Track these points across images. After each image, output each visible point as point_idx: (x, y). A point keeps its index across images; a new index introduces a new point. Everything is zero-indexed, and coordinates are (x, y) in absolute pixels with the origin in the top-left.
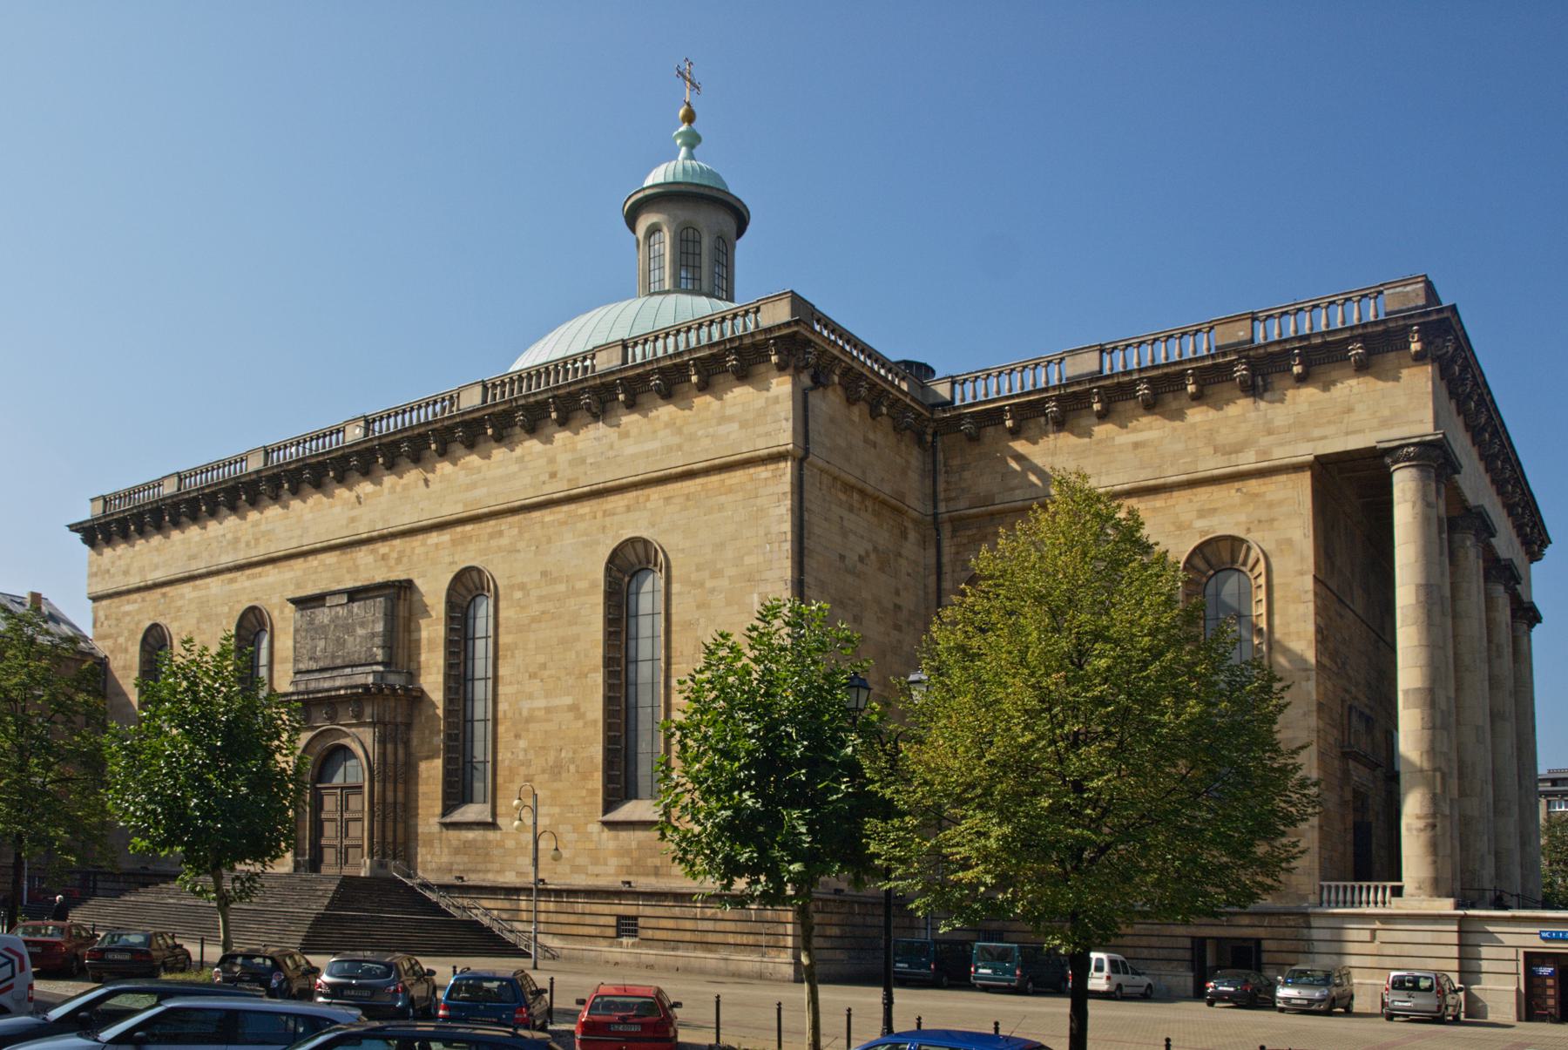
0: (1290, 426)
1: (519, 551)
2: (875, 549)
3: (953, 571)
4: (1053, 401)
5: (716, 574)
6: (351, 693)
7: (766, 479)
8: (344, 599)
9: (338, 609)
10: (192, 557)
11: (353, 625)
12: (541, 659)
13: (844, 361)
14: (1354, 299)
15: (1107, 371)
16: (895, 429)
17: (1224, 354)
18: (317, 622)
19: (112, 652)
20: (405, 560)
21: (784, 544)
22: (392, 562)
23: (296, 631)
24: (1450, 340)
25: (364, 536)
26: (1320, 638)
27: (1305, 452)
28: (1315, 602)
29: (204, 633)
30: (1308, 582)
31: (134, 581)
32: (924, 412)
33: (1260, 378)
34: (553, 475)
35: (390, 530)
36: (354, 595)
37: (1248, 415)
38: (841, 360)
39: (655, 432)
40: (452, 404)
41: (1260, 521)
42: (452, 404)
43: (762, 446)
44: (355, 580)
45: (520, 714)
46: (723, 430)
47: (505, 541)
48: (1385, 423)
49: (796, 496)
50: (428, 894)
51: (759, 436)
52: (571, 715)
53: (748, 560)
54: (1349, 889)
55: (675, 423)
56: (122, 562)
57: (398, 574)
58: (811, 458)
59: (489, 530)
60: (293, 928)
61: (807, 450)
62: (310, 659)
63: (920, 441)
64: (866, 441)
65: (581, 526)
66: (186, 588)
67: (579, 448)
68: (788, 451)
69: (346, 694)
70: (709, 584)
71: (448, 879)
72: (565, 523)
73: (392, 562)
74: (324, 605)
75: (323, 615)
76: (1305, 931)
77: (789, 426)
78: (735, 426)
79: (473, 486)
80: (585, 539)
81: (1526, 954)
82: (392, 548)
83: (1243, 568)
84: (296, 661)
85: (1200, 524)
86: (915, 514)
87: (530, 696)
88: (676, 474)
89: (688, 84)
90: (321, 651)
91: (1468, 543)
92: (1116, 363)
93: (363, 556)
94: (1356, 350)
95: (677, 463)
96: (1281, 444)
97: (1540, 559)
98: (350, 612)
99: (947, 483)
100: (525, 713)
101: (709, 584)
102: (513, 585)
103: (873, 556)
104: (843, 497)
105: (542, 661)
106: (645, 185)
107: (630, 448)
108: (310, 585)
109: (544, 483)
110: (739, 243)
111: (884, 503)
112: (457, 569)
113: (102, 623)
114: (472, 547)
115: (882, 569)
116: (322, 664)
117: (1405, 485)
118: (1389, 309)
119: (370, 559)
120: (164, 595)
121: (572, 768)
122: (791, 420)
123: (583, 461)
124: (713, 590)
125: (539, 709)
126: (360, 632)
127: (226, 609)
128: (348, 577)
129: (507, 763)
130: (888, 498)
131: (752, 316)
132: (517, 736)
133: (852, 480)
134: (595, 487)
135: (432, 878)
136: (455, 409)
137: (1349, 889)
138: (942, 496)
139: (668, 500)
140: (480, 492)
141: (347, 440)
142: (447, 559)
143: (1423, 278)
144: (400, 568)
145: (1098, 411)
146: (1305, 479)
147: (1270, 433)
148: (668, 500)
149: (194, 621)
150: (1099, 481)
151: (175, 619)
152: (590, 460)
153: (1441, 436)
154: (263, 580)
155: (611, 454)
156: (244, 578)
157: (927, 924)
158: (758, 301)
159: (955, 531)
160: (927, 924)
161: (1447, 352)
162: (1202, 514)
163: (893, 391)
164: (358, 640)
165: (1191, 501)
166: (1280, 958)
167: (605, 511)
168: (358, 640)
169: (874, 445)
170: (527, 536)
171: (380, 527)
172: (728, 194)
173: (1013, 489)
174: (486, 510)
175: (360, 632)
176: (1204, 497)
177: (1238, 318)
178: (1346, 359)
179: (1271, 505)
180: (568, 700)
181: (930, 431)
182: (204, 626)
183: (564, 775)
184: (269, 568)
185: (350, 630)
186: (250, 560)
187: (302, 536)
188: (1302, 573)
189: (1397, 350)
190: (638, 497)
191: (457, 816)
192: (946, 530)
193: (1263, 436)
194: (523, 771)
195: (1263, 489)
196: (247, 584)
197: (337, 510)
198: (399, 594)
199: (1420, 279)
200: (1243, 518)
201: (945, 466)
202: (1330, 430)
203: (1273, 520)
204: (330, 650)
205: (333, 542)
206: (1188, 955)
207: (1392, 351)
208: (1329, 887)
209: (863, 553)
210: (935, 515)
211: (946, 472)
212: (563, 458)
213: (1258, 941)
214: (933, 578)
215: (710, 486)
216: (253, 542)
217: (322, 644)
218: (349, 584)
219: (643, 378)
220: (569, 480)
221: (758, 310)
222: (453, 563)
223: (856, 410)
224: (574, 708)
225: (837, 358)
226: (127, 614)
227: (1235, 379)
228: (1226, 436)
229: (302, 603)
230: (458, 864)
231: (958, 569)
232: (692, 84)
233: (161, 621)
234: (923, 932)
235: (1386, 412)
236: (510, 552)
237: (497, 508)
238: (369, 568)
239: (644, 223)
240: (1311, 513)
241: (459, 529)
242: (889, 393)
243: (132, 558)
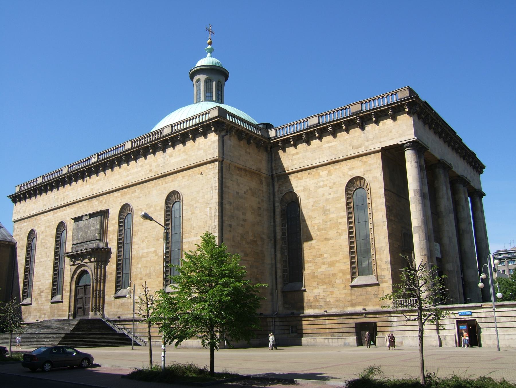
0: (374, 138)
1: (140, 197)
2: (250, 189)
3: (278, 194)
4: (330, 127)
5: (197, 202)
6: (88, 251)
7: (211, 168)
8: (88, 217)
9: (86, 221)
10: (44, 205)
11: (90, 226)
12: (146, 235)
13: (236, 127)
14: (328, 114)
15: (321, 123)
16: (257, 147)
17: (352, 116)
18: (80, 226)
19: (18, 240)
20: (107, 202)
21: (216, 190)
22: (103, 203)
23: (73, 230)
24: (417, 107)
25: (95, 195)
26: (388, 210)
27: (378, 146)
28: (385, 198)
29: (47, 232)
30: (382, 191)
31: (27, 215)
32: (266, 141)
33: (364, 123)
34: (151, 171)
35: (103, 192)
36: (91, 216)
37: (361, 135)
38: (235, 127)
39: (180, 155)
40: (161, 134)
41: (367, 171)
42: (161, 134)
43: (209, 158)
44: (92, 210)
45: (139, 255)
46: (199, 153)
47: (136, 194)
48: (401, 136)
49: (220, 174)
50: (109, 323)
51: (209, 154)
52: (154, 255)
53: (206, 197)
54: (412, 301)
55: (185, 151)
56: (24, 208)
57: (104, 208)
58: (225, 160)
59: (132, 191)
60: (57, 339)
61: (223, 158)
62: (77, 239)
63: (266, 150)
64: (246, 152)
65: (159, 187)
66: (42, 216)
67: (158, 161)
68: (217, 159)
69: (86, 252)
70: (195, 205)
71: (116, 318)
72: (154, 187)
73: (103, 203)
74: (82, 220)
75: (82, 223)
76: (390, 318)
77: (217, 150)
78: (202, 151)
79: (128, 176)
80: (159, 192)
81: (457, 321)
82: (104, 198)
83: (364, 187)
84: (73, 240)
85: (350, 173)
86: (265, 175)
87: (142, 249)
88: (186, 168)
89: (210, 33)
90: (80, 236)
91: (441, 172)
92: (323, 120)
93: (95, 201)
94: (390, 112)
95: (185, 165)
96: (371, 144)
97: (482, 173)
98: (89, 222)
99: (275, 164)
100: (141, 255)
101: (195, 205)
102: (138, 209)
103: (249, 192)
104: (238, 172)
105: (146, 236)
106: (196, 66)
107: (173, 160)
108: (79, 213)
109: (148, 173)
110: (226, 83)
111: (253, 173)
112: (122, 204)
113: (16, 230)
114: (127, 196)
115: (253, 196)
116: (80, 241)
117: (410, 156)
118: (399, 98)
119: (97, 202)
120: (36, 219)
121: (154, 274)
122: (218, 148)
123: (159, 166)
124: (196, 207)
125: (145, 253)
126: (92, 228)
127: (53, 223)
128: (90, 209)
129: (135, 273)
130: (255, 171)
131: (207, 114)
132: (138, 263)
133: (241, 166)
134: (162, 174)
135: (111, 318)
136: (162, 135)
137: (412, 301)
138: (274, 168)
139: (183, 177)
140: (130, 177)
141: (164, 134)
142: (120, 201)
143: (408, 88)
144: (106, 205)
145: (407, 111)
146: (379, 155)
147: (368, 141)
148: (183, 177)
149: (44, 228)
150: (319, 160)
151: (38, 228)
152: (161, 165)
153: (416, 139)
154: (65, 212)
155: (167, 162)
156: (60, 212)
157: (273, 324)
158: (209, 110)
159: (278, 180)
160: (273, 324)
161: (417, 111)
162: (351, 169)
163: (255, 135)
164: (91, 231)
165: (347, 165)
166: (383, 329)
167: (165, 182)
168: (91, 231)
169: (249, 153)
170: (143, 192)
171: (100, 191)
172: (223, 68)
173: (294, 165)
174: (131, 184)
175: (92, 228)
176: (350, 164)
177: (356, 103)
178: (355, 124)
179: (370, 165)
180: (153, 249)
181: (269, 147)
182: (47, 229)
183: (152, 277)
184: (67, 207)
185: (89, 228)
186: (61, 205)
187: (77, 196)
188: (380, 188)
189: (402, 111)
190: (175, 177)
191: (119, 293)
192: (276, 179)
193: (366, 142)
194: (139, 276)
195: (367, 160)
196: (60, 213)
197: (88, 186)
198: (104, 214)
199: (407, 88)
200: (362, 170)
201: (275, 158)
202: (385, 139)
203: (370, 170)
204: (83, 236)
205: (86, 197)
206: (354, 330)
207: (401, 111)
208: (413, 300)
209: (246, 191)
210: (272, 175)
211: (275, 160)
212: (154, 165)
213: (375, 323)
214: (272, 197)
215: (196, 172)
216: (63, 199)
217: (81, 234)
218: (90, 212)
219: (138, 151)
220: (155, 172)
221: (209, 113)
222: (121, 203)
223: (242, 142)
224: (155, 252)
225: (233, 126)
226: (24, 226)
227: (329, 131)
228: (355, 143)
229: (77, 219)
230: (119, 312)
231: (279, 193)
232: (212, 32)
233: (34, 228)
234: (272, 327)
235: (401, 132)
236: (138, 198)
237: (134, 183)
238: (96, 206)
239: (196, 78)
240: (382, 168)
241: (123, 190)
242: (253, 136)
243: (27, 206)
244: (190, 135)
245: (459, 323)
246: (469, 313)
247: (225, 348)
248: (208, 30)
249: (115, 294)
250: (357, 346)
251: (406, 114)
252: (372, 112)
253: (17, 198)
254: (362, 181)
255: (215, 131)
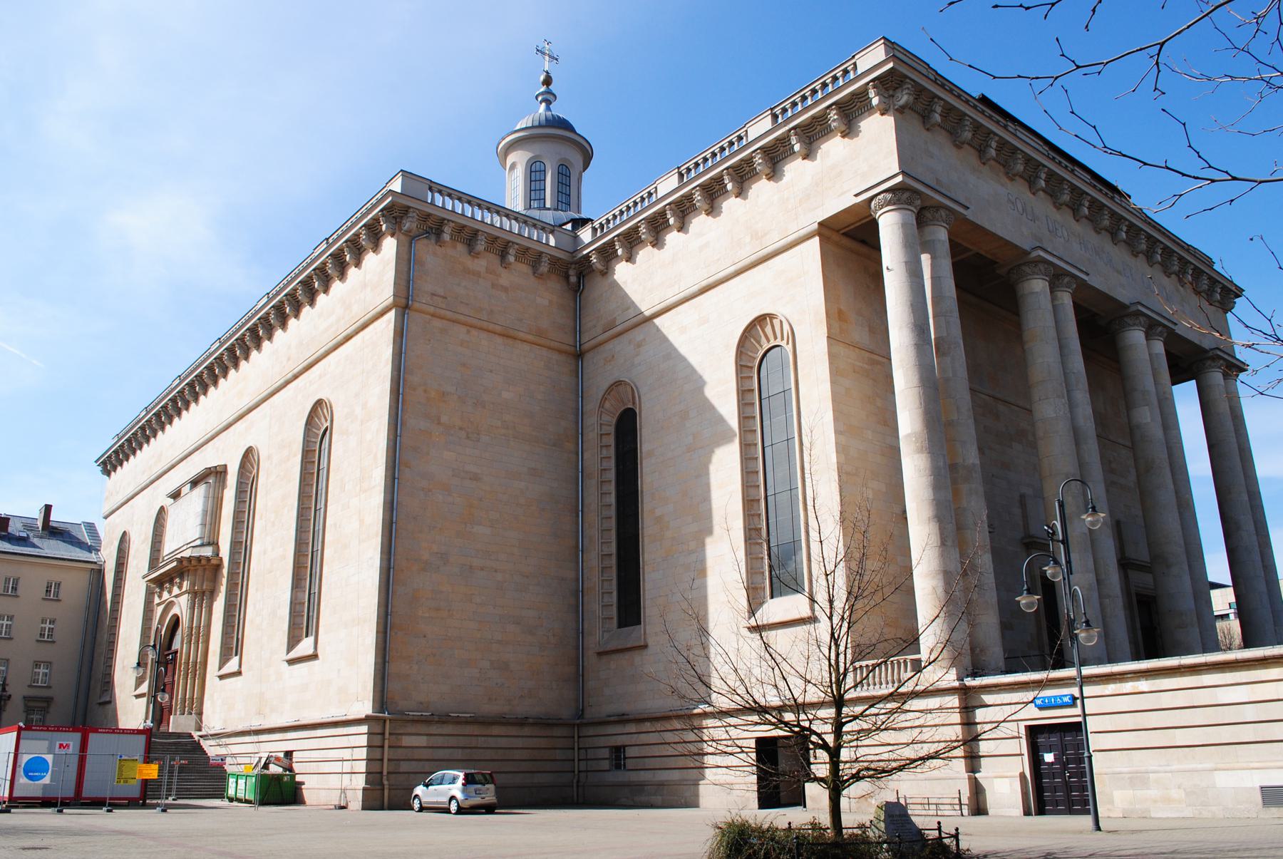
89: (547, 58)
117: (890, 226)
143: (882, 41)
198: (219, 473)
239: (511, 159)
244: (346, 254)
245: (1035, 733)
246: (1066, 699)
247: (382, 809)
248: (553, 58)
249: (220, 669)
250: (759, 808)
251: (877, 115)
252: (787, 128)
253: (110, 464)
254: (776, 322)
255: (392, 235)
